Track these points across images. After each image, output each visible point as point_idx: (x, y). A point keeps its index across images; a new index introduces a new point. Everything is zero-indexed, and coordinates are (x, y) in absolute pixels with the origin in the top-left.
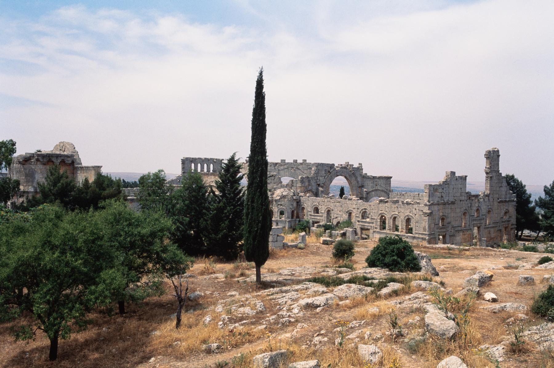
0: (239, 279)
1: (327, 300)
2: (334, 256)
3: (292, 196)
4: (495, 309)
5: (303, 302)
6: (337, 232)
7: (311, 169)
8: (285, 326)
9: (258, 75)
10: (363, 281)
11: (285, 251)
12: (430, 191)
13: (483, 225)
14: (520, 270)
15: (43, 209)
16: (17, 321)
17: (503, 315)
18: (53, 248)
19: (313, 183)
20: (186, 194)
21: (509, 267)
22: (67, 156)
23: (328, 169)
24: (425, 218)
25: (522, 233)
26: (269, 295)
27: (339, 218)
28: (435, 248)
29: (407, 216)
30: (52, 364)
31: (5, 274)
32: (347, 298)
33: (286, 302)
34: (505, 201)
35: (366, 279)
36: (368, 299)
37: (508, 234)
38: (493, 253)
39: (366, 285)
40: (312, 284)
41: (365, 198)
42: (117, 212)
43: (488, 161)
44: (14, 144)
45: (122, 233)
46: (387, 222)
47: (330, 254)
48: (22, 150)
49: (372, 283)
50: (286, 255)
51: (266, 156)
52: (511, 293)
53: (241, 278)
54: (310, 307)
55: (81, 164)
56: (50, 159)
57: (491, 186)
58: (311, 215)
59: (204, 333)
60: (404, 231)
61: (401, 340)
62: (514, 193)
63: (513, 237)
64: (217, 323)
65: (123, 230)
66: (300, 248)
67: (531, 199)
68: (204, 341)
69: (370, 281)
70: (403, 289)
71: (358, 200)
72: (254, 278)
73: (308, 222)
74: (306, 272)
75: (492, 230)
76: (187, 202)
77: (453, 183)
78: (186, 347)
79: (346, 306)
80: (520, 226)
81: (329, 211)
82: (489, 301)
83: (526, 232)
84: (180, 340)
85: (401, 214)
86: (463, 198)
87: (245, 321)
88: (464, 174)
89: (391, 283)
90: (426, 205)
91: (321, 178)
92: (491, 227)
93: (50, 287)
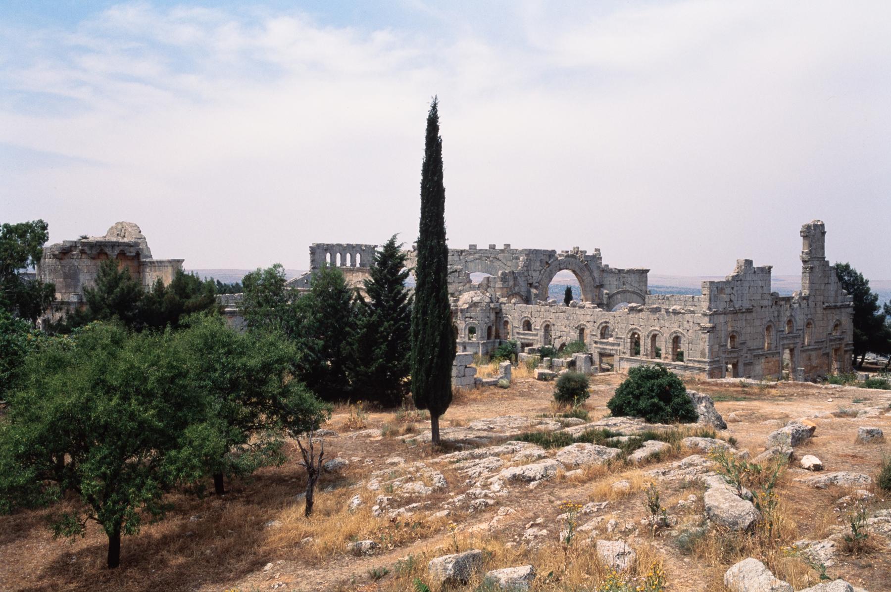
1: (546, 469)
2: (556, 398)
3: (488, 303)
4: (819, 482)
5: (507, 473)
6: (561, 360)
7: (517, 258)
9: (430, 109)
10: (605, 438)
11: (478, 392)
12: (711, 291)
13: (799, 345)
15: (93, 330)
17: (833, 491)
19: (521, 281)
21: (842, 414)
22: (129, 245)
24: (703, 336)
26: (453, 462)
27: (564, 338)
28: (721, 384)
29: (675, 332)
30: (112, 573)
32: (577, 465)
33: (480, 473)
34: (835, 307)
35: (608, 435)
36: (612, 467)
37: (840, 360)
38: (815, 391)
39: (609, 445)
40: (521, 444)
41: (606, 304)
42: (208, 333)
43: (807, 242)
44: (45, 227)
45: (217, 366)
46: (642, 343)
47: (551, 396)
48: (56, 238)
49: (618, 442)
50: (479, 397)
51: (444, 240)
53: (408, 436)
54: (518, 480)
55: (151, 257)
56: (102, 250)
58: (518, 333)
59: (351, 523)
60: (670, 357)
61: (667, 532)
64: (371, 507)
65: (219, 361)
66: (502, 387)
67: (878, 303)
68: (350, 537)
69: (615, 439)
70: (669, 450)
71: (594, 308)
72: (429, 435)
73: (514, 345)
75: (813, 353)
76: (319, 315)
77: (748, 278)
78: (322, 545)
79: (577, 479)
80: (860, 348)
81: (547, 327)
82: (808, 469)
83: (870, 357)
84: (312, 535)
86: (765, 303)
87: (414, 505)
89: (650, 442)
90: (705, 315)
91: (534, 274)
92: (812, 350)
93: (106, 452)
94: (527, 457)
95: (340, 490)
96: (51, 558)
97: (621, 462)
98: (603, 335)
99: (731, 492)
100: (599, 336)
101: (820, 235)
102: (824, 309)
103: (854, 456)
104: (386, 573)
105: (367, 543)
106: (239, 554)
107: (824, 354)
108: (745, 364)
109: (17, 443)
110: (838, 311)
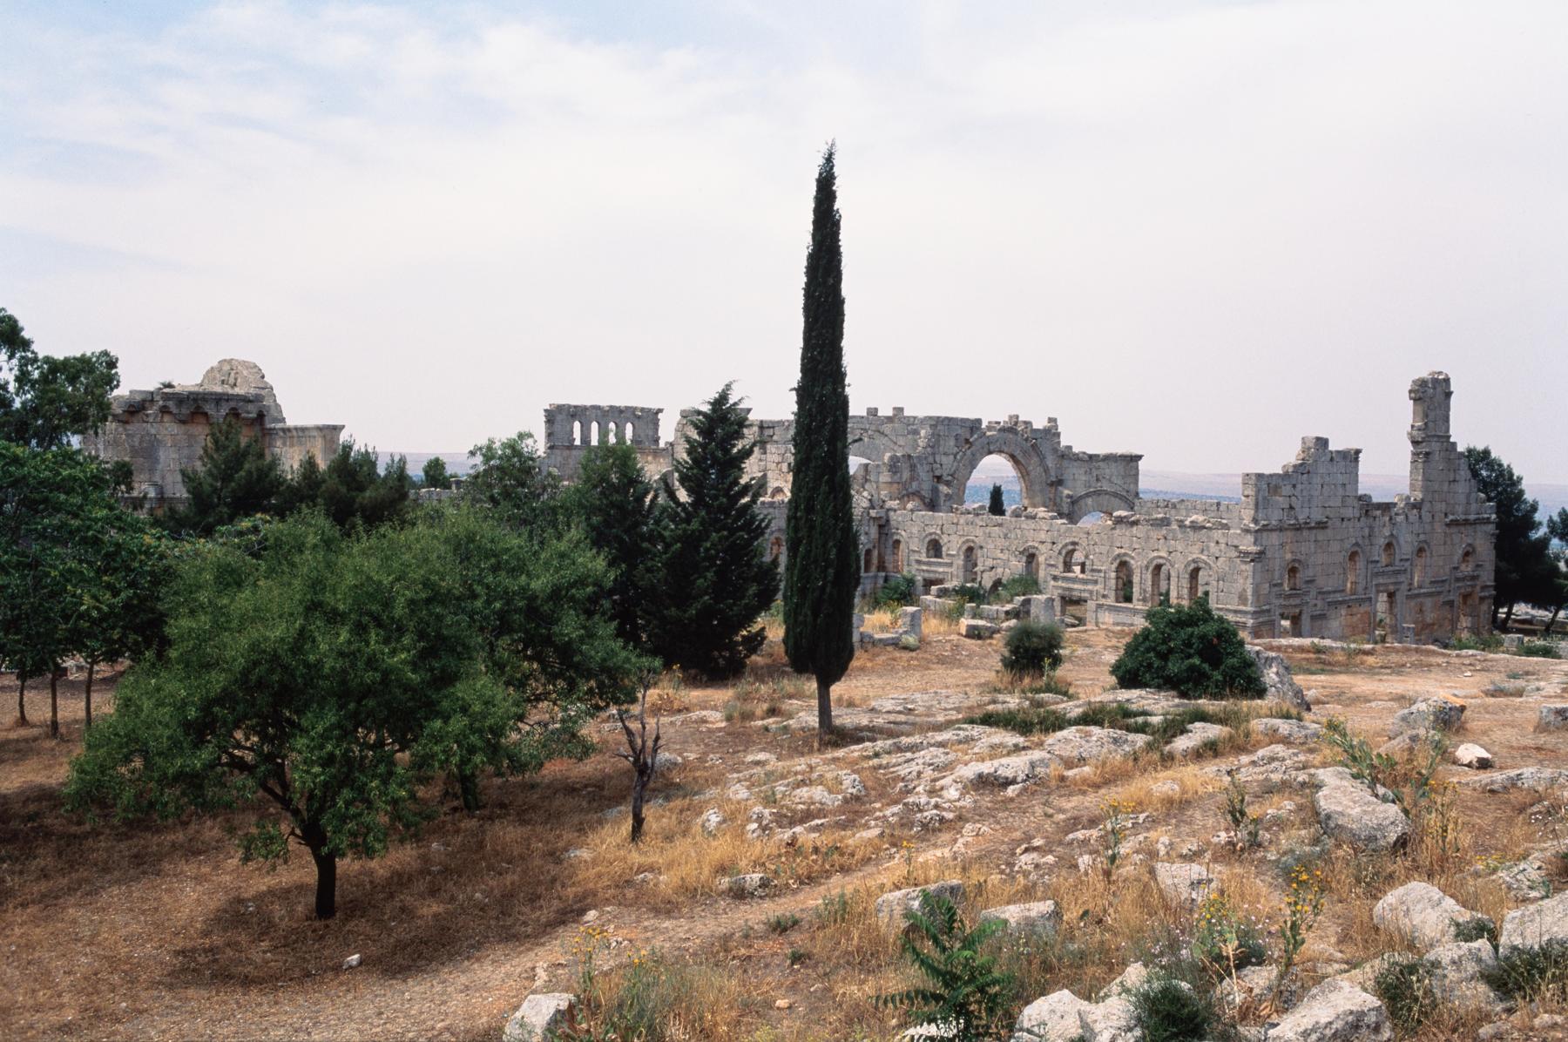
0: (765, 722)
1: (1033, 765)
2: (1006, 666)
4: (1492, 782)
5: (970, 771)
6: (995, 607)
7: (916, 432)
8: (931, 830)
9: (822, 161)
11: (865, 655)
12: (1258, 491)
13: (1404, 587)
14: (1531, 700)
15: (256, 530)
16: (193, 827)
17: (1516, 797)
18: (334, 618)
19: (923, 472)
20: (595, 496)
21: (1498, 692)
22: (246, 400)
23: (965, 433)
24: (1243, 567)
25: (1509, 613)
26: (869, 758)
27: (1000, 570)
28: (1279, 649)
29: (1194, 561)
30: (327, 926)
31: (218, 688)
32: (1082, 761)
33: (919, 773)
34: (1466, 522)
35: (1127, 714)
36: (1141, 763)
37: (1474, 615)
38: (1440, 660)
39: (1129, 729)
40: (981, 728)
42: (462, 534)
43: (1420, 408)
44: (112, 364)
45: (478, 589)
46: (1136, 579)
48: (133, 380)
49: (1146, 724)
52: (1525, 748)
53: (771, 720)
54: (984, 783)
55: (283, 420)
56: (198, 407)
57: (1426, 479)
58: (919, 562)
59: (721, 849)
62: (1490, 499)
63: (1485, 618)
64: (743, 826)
65: (480, 582)
66: (906, 648)
67: (1537, 517)
68: (722, 870)
69: (1140, 720)
70: (1231, 737)
71: (1053, 518)
72: (813, 720)
73: (910, 582)
74: (943, 705)
75: (1428, 602)
76: (595, 520)
79: (1084, 781)
80: (1506, 593)
81: (970, 549)
82: (1469, 765)
83: (1522, 610)
85: (1176, 557)
86: (1349, 513)
88: (1354, 446)
89: (1198, 724)
90: (1247, 531)
91: (944, 460)
92: (1426, 595)
93: (333, 719)
94: (992, 747)
95: (678, 803)
96: (212, 905)
97: (1156, 756)
98: (1068, 566)
99: (1361, 792)
100: (1061, 566)
101: (1443, 397)
102: (1447, 525)
103: (1538, 749)
104: (796, 923)
105: (755, 877)
106: (534, 899)
107: (1445, 603)
108: (1314, 618)
109: (183, 706)
110: (1470, 529)
